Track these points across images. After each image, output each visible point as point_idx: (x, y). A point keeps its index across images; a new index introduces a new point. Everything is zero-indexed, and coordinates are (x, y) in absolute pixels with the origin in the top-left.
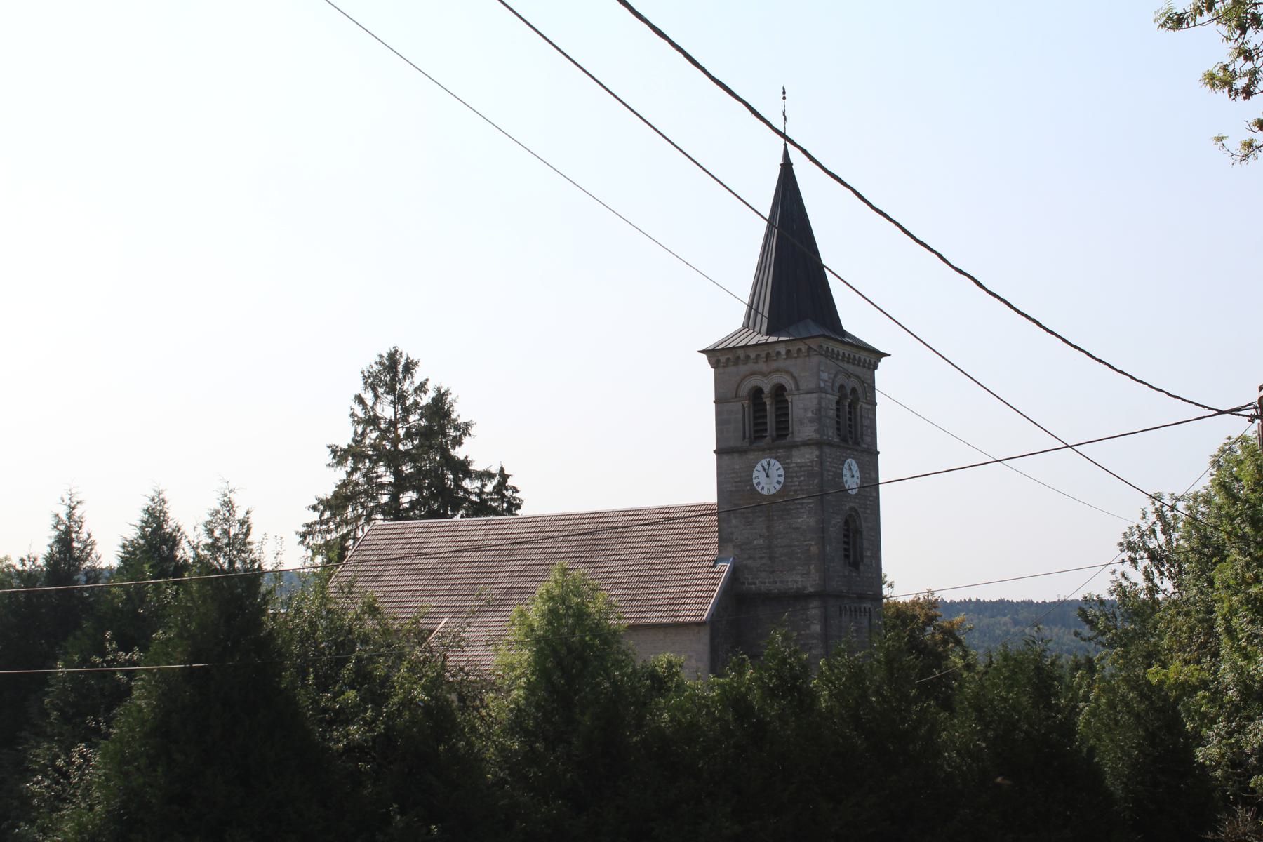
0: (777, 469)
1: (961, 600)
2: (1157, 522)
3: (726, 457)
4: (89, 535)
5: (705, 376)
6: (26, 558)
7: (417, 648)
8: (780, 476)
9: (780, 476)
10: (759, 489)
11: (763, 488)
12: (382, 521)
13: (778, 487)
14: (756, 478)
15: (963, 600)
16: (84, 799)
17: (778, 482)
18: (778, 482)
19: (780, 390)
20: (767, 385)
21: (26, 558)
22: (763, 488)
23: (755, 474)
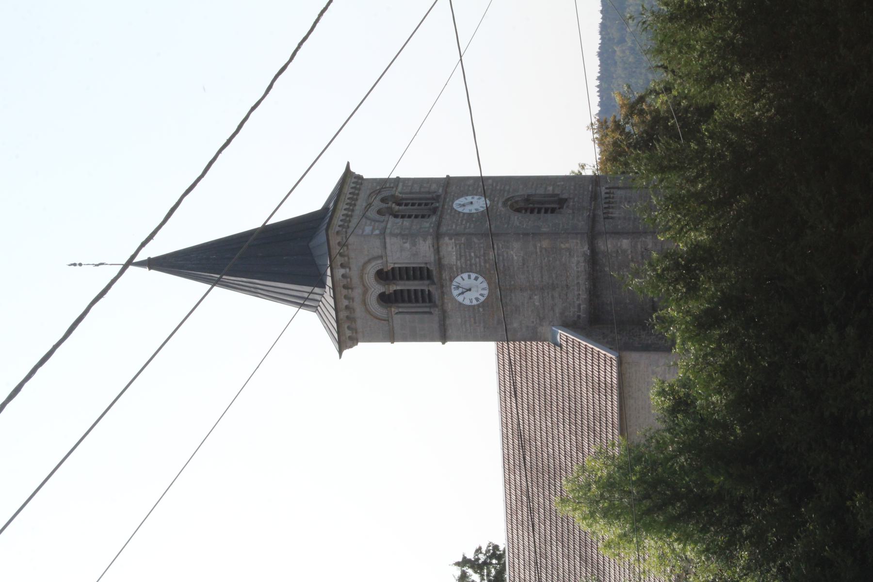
8: (469, 277)
9: (469, 277)
10: (482, 299)
13: (481, 279)
14: (471, 301)
17: (476, 279)
18: (476, 279)
19: (382, 276)
20: (377, 289)
22: (482, 295)
23: (467, 302)
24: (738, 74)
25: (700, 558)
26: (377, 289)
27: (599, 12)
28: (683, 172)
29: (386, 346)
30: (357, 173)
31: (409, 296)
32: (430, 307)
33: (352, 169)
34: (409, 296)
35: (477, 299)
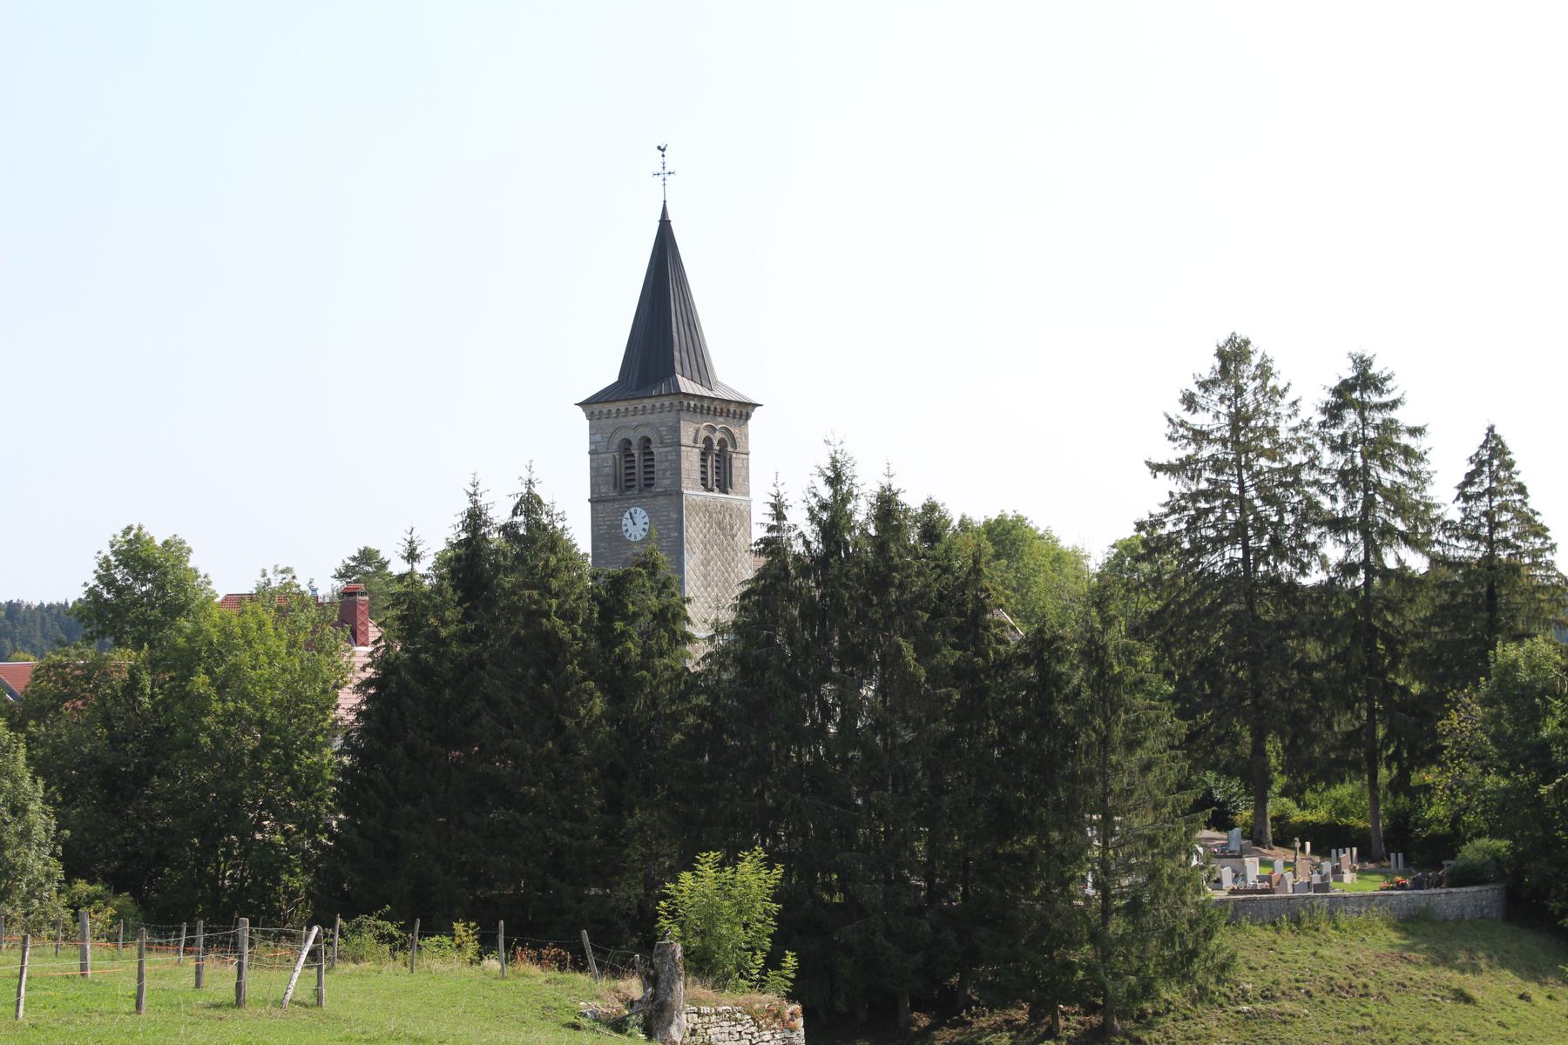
0: (641, 515)
1: (42, 604)
2: (1289, 509)
3: (600, 507)
4: (429, 568)
5: (579, 428)
6: (1195, 389)
7: (748, 1017)
8: (645, 523)
9: (645, 523)
10: (627, 535)
11: (630, 535)
12: (1406, 478)
13: (644, 534)
14: (626, 525)
15: (46, 604)
16: (105, 695)
17: (644, 530)
18: (644, 530)
19: (647, 441)
20: (635, 439)
21: (1195, 389)
22: (630, 535)
23: (624, 522)
24: (1378, 1026)
25: (1096, 913)
26: (635, 439)
27: (347, 552)
28: (423, 656)
29: (586, 446)
30: (753, 414)
31: (649, 473)
32: (621, 487)
33: (757, 409)
34: (649, 473)
35: (627, 531)
